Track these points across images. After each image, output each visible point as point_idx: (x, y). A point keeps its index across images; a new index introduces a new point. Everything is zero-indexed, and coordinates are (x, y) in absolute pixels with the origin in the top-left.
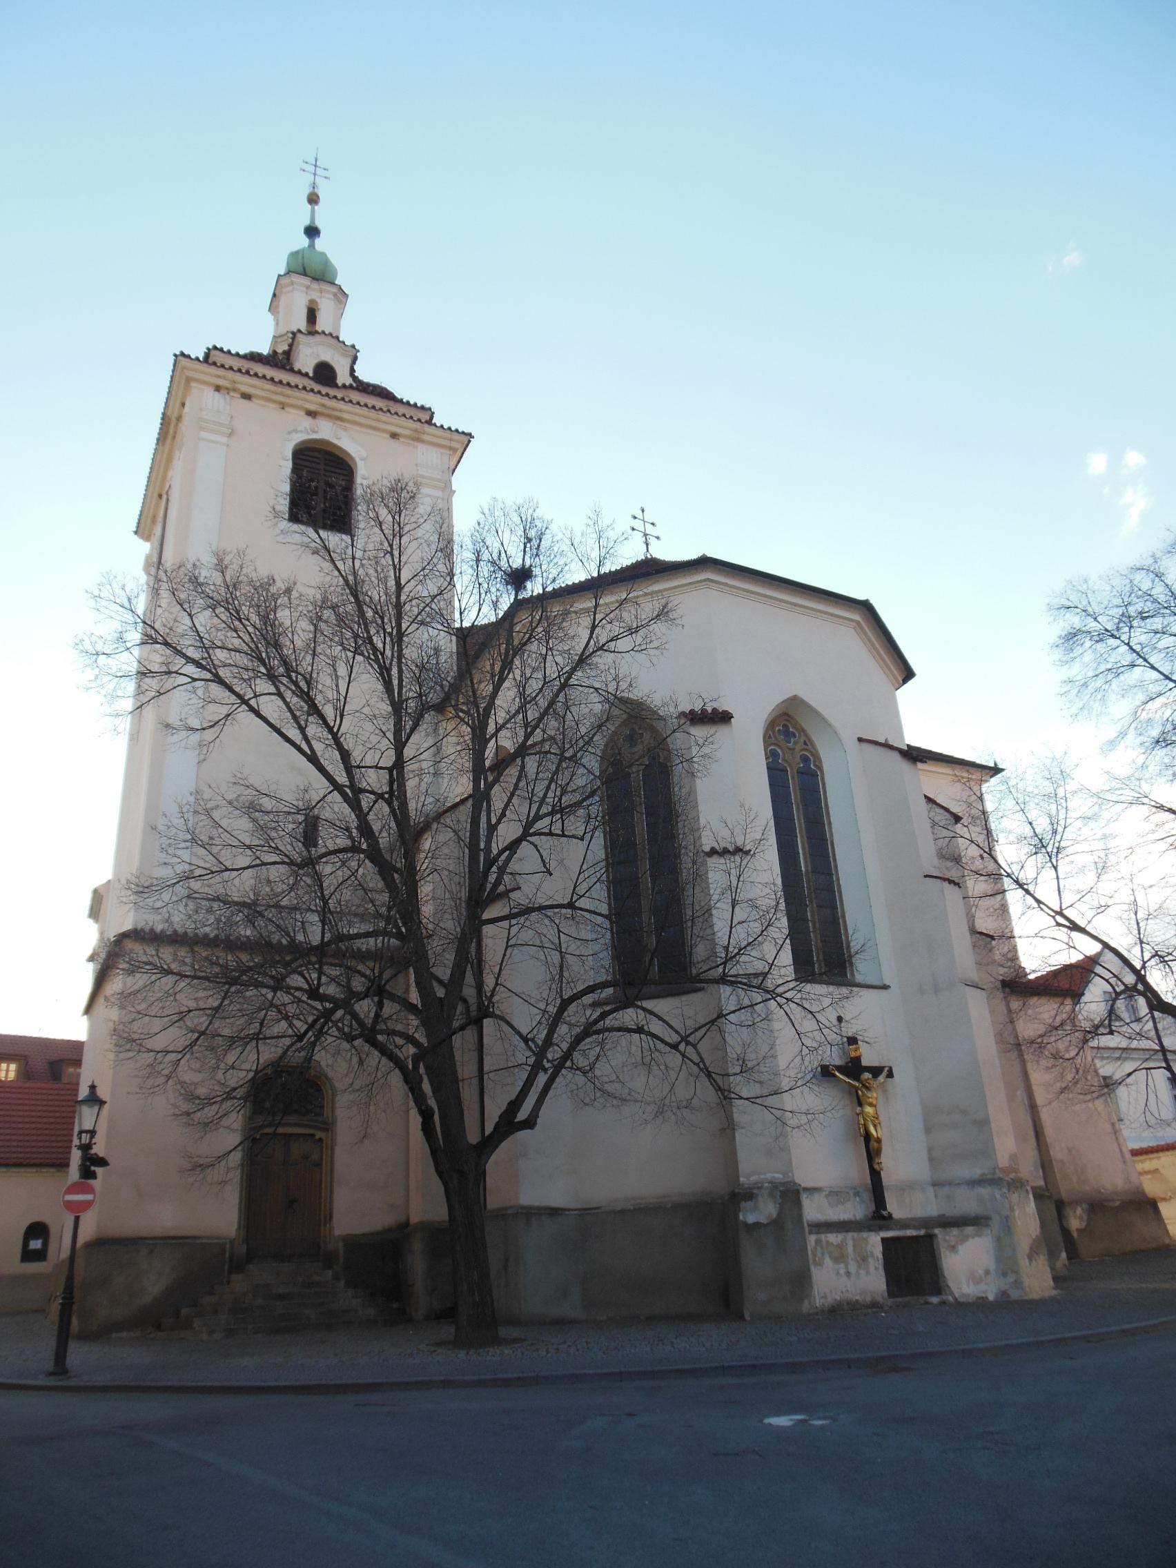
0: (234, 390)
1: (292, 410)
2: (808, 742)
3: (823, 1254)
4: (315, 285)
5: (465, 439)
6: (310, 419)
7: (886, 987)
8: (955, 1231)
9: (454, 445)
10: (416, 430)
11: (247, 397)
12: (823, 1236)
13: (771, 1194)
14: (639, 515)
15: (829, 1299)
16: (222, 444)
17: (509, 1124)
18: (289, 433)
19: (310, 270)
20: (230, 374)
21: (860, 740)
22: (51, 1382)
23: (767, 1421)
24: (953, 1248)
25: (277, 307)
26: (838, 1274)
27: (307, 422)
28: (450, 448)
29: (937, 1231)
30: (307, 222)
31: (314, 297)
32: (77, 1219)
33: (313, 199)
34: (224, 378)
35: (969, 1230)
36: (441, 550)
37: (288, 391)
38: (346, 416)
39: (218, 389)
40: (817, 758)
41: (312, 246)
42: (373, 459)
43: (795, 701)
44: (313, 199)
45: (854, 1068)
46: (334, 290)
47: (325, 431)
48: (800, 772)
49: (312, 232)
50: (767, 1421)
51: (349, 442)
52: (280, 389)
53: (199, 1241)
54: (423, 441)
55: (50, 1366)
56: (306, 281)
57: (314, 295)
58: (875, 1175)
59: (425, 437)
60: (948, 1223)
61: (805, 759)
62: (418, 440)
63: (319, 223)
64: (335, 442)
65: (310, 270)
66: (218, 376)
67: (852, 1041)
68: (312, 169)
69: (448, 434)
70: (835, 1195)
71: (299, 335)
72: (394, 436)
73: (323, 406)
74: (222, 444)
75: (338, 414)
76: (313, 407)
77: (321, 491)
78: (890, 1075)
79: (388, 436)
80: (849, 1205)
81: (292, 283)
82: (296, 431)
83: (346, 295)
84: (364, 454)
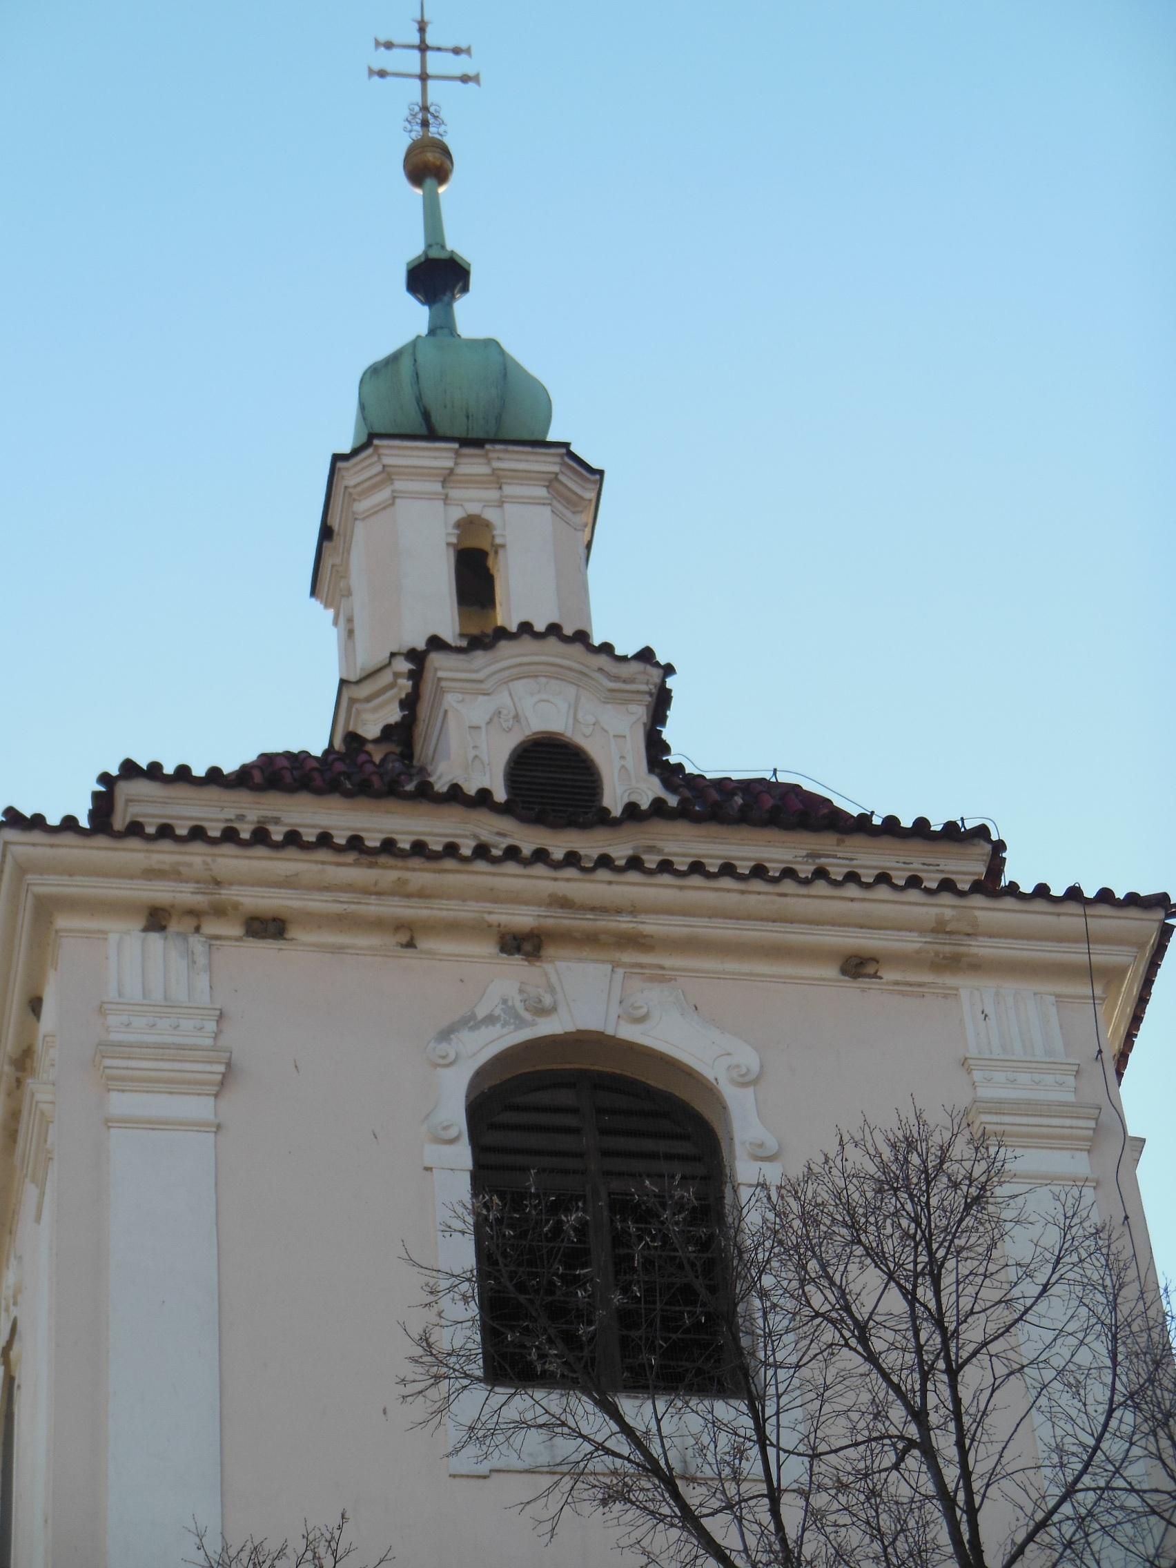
0: (219, 911)
4: (474, 465)
5: (1148, 923)
6: (516, 966)
9: (1104, 956)
10: (939, 928)
11: (267, 927)
18: (445, 1035)
19: (450, 415)
20: (196, 857)
23: (103, 789)
25: (342, 573)
28: (1091, 973)
30: (415, 248)
33: (428, 165)
34: (172, 874)
37: (420, 876)
38: (652, 926)
39: (157, 919)
41: (442, 327)
44: (428, 165)
46: (546, 464)
50: (88, 826)
52: (387, 874)
54: (977, 967)
56: (438, 457)
57: (473, 501)
59: (982, 948)
62: (953, 963)
63: (457, 243)
64: (629, 1033)
65: (450, 415)
66: (152, 874)
68: (411, 61)
69: (1071, 918)
71: (437, 660)
72: (857, 966)
73: (564, 903)
75: (624, 924)
76: (523, 919)
81: (388, 475)
82: (470, 1022)
83: (601, 473)
84: (749, 1059)
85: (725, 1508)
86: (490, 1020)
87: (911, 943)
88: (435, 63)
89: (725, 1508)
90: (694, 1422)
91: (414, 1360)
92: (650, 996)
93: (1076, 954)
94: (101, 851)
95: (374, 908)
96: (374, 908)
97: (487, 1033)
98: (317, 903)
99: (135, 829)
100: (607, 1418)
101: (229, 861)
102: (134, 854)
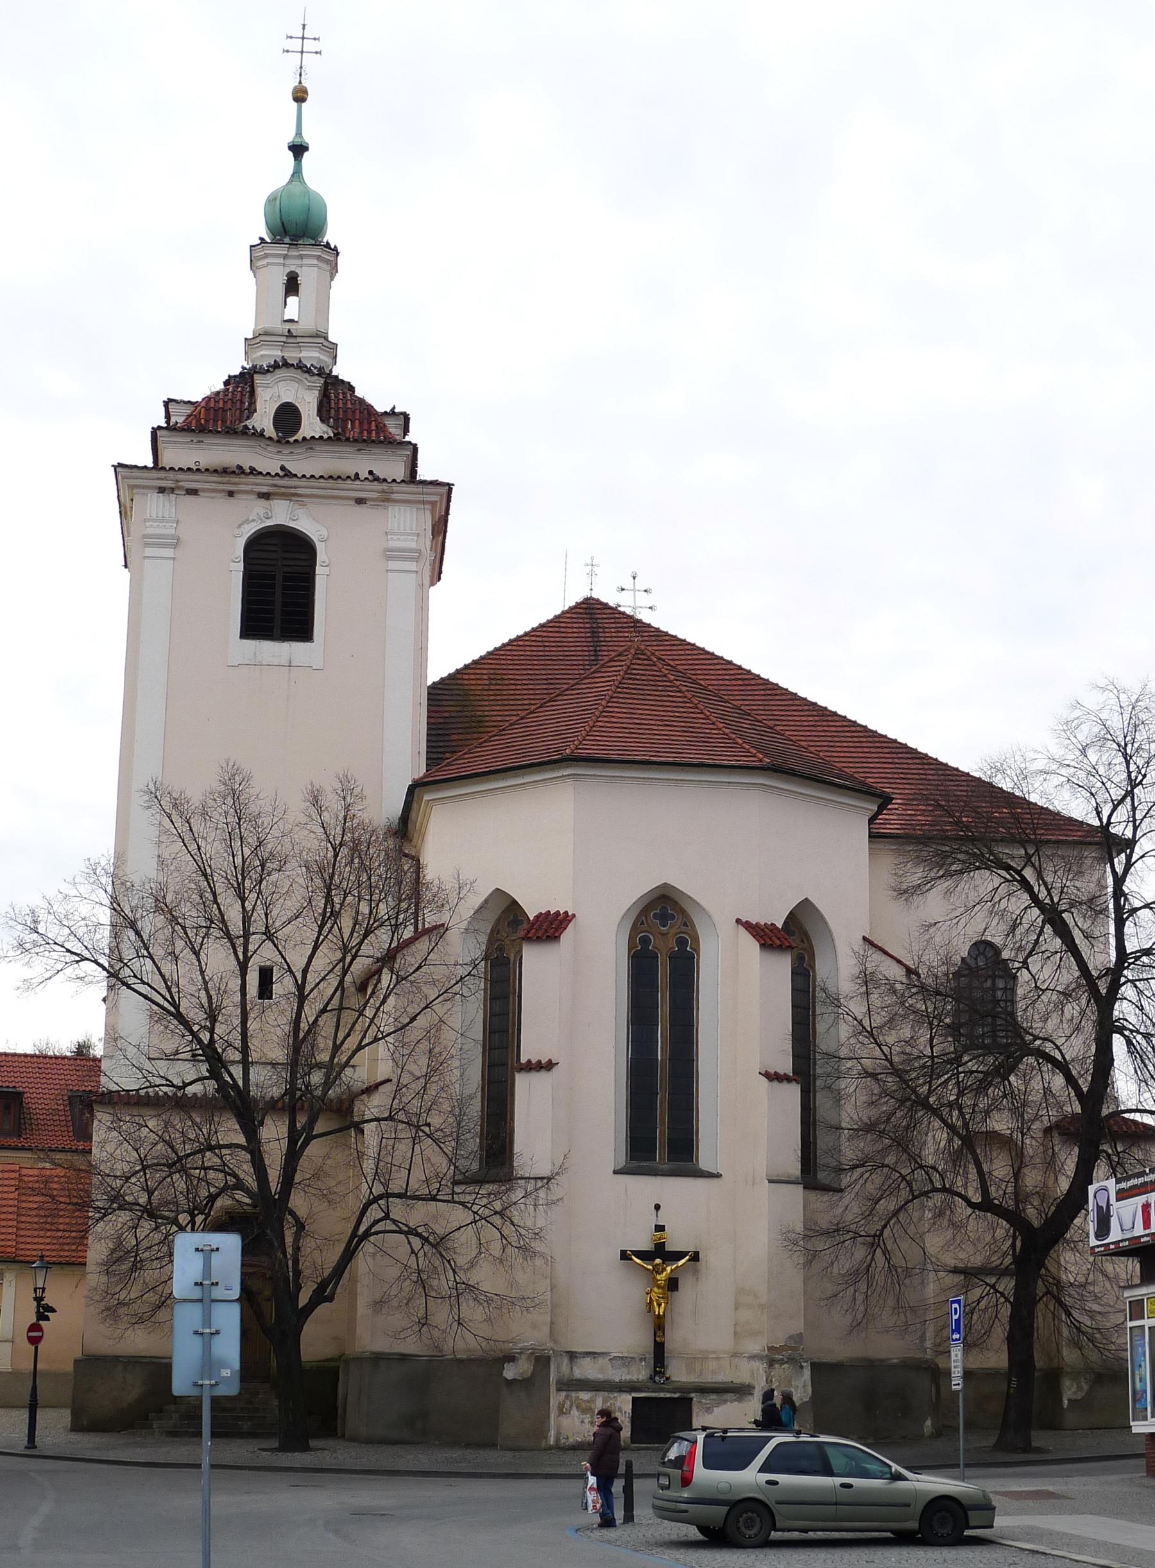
0: (179, 488)
1: (244, 496)
2: (688, 923)
3: (571, 1406)
6: (262, 502)
7: (718, 1176)
8: (713, 1396)
10: (383, 491)
11: (193, 492)
12: (573, 1394)
13: (528, 1358)
14: (628, 583)
15: (571, 1440)
16: (279, 264)
17: (322, 1295)
18: (240, 526)
19: (296, 231)
20: (171, 475)
21: (738, 921)
22: (28, 1452)
24: (709, 1410)
26: (582, 1422)
27: (260, 507)
29: (693, 1395)
30: (290, 137)
31: (293, 268)
32: (36, 1349)
33: (300, 96)
34: (166, 479)
35: (729, 1396)
36: (170, 954)
38: (299, 491)
39: (162, 490)
40: (696, 940)
41: (297, 173)
42: (347, 551)
43: (665, 886)
44: (300, 96)
45: (660, 1253)
47: (281, 514)
48: (673, 957)
49: (298, 150)
51: (305, 522)
53: (164, 1361)
54: (395, 501)
55: (25, 1443)
58: (659, 1350)
59: (394, 496)
60: (704, 1390)
61: (682, 942)
62: (388, 500)
63: (308, 137)
65: (296, 231)
67: (660, 1228)
68: (296, 45)
70: (626, 1361)
72: (360, 501)
73: (276, 486)
74: (279, 264)
75: (293, 491)
76: (264, 489)
77: (279, 594)
78: (695, 1257)
79: (353, 502)
80: (633, 1369)
82: (247, 521)
84: (325, 533)
85: (200, 1301)
86: (254, 520)
87: (374, 495)
88: (309, 45)
89: (200, 1301)
90: (1073, 805)
91: (315, 800)
92: (300, 511)
93: (420, 497)
94: (155, 474)
95: (222, 487)
96: (222, 487)
97: (254, 524)
98: (206, 486)
99: (163, 468)
100: (1051, 808)
101: (180, 476)
102: (162, 474)
